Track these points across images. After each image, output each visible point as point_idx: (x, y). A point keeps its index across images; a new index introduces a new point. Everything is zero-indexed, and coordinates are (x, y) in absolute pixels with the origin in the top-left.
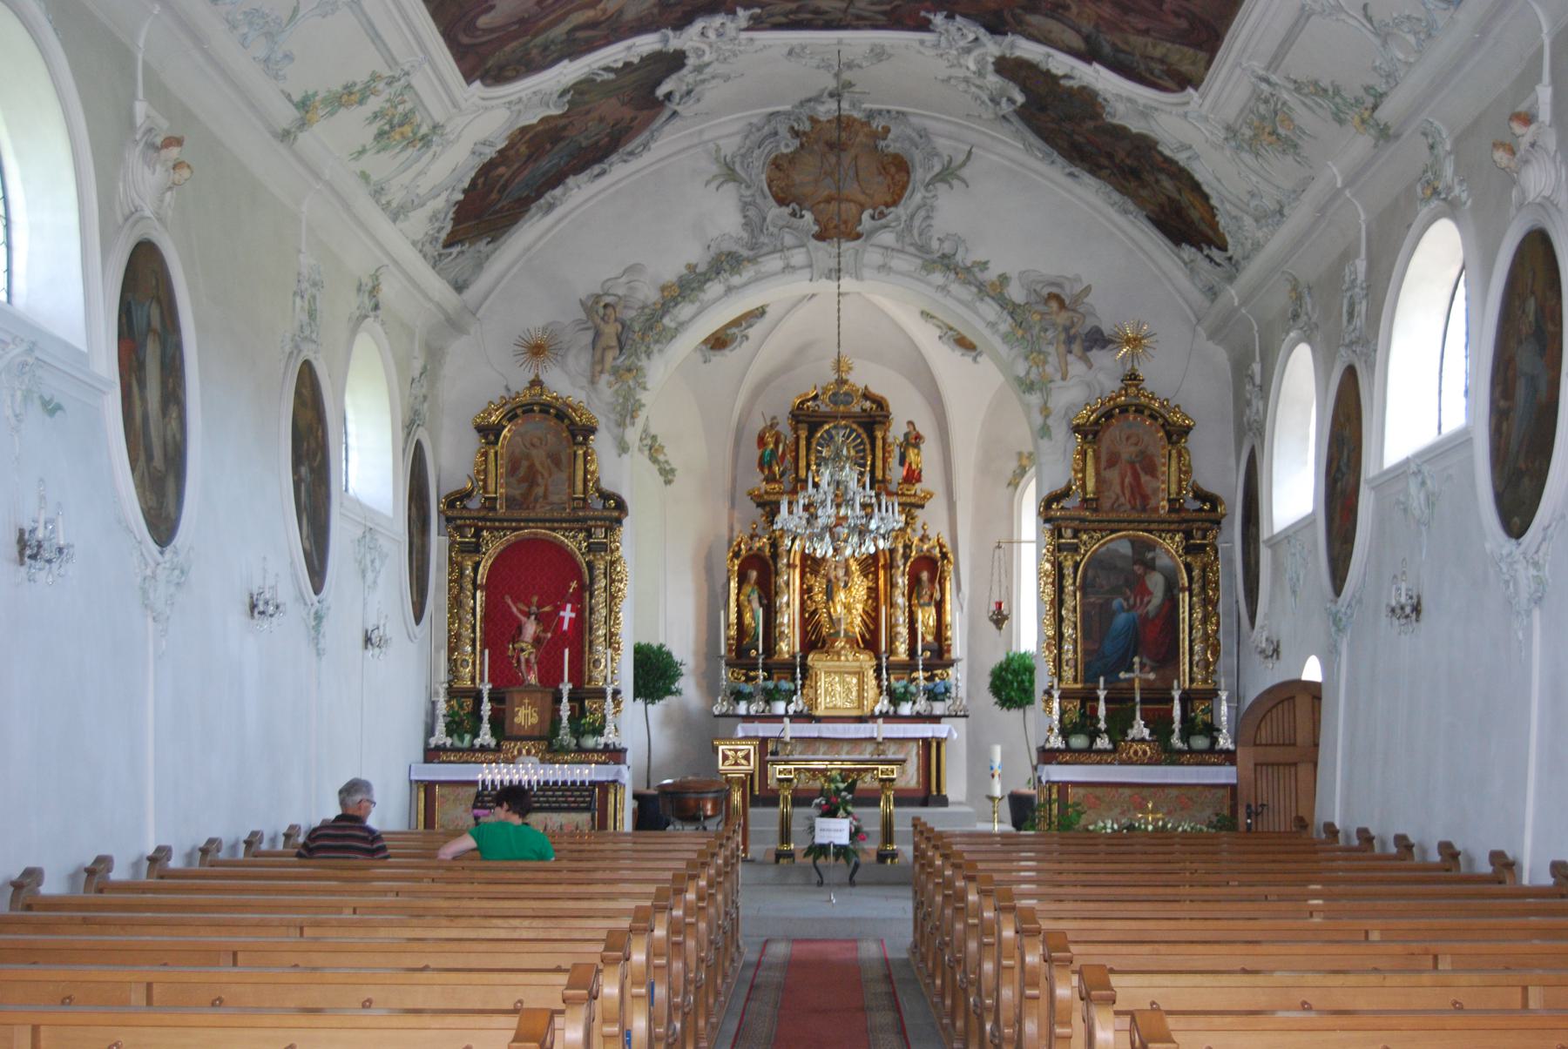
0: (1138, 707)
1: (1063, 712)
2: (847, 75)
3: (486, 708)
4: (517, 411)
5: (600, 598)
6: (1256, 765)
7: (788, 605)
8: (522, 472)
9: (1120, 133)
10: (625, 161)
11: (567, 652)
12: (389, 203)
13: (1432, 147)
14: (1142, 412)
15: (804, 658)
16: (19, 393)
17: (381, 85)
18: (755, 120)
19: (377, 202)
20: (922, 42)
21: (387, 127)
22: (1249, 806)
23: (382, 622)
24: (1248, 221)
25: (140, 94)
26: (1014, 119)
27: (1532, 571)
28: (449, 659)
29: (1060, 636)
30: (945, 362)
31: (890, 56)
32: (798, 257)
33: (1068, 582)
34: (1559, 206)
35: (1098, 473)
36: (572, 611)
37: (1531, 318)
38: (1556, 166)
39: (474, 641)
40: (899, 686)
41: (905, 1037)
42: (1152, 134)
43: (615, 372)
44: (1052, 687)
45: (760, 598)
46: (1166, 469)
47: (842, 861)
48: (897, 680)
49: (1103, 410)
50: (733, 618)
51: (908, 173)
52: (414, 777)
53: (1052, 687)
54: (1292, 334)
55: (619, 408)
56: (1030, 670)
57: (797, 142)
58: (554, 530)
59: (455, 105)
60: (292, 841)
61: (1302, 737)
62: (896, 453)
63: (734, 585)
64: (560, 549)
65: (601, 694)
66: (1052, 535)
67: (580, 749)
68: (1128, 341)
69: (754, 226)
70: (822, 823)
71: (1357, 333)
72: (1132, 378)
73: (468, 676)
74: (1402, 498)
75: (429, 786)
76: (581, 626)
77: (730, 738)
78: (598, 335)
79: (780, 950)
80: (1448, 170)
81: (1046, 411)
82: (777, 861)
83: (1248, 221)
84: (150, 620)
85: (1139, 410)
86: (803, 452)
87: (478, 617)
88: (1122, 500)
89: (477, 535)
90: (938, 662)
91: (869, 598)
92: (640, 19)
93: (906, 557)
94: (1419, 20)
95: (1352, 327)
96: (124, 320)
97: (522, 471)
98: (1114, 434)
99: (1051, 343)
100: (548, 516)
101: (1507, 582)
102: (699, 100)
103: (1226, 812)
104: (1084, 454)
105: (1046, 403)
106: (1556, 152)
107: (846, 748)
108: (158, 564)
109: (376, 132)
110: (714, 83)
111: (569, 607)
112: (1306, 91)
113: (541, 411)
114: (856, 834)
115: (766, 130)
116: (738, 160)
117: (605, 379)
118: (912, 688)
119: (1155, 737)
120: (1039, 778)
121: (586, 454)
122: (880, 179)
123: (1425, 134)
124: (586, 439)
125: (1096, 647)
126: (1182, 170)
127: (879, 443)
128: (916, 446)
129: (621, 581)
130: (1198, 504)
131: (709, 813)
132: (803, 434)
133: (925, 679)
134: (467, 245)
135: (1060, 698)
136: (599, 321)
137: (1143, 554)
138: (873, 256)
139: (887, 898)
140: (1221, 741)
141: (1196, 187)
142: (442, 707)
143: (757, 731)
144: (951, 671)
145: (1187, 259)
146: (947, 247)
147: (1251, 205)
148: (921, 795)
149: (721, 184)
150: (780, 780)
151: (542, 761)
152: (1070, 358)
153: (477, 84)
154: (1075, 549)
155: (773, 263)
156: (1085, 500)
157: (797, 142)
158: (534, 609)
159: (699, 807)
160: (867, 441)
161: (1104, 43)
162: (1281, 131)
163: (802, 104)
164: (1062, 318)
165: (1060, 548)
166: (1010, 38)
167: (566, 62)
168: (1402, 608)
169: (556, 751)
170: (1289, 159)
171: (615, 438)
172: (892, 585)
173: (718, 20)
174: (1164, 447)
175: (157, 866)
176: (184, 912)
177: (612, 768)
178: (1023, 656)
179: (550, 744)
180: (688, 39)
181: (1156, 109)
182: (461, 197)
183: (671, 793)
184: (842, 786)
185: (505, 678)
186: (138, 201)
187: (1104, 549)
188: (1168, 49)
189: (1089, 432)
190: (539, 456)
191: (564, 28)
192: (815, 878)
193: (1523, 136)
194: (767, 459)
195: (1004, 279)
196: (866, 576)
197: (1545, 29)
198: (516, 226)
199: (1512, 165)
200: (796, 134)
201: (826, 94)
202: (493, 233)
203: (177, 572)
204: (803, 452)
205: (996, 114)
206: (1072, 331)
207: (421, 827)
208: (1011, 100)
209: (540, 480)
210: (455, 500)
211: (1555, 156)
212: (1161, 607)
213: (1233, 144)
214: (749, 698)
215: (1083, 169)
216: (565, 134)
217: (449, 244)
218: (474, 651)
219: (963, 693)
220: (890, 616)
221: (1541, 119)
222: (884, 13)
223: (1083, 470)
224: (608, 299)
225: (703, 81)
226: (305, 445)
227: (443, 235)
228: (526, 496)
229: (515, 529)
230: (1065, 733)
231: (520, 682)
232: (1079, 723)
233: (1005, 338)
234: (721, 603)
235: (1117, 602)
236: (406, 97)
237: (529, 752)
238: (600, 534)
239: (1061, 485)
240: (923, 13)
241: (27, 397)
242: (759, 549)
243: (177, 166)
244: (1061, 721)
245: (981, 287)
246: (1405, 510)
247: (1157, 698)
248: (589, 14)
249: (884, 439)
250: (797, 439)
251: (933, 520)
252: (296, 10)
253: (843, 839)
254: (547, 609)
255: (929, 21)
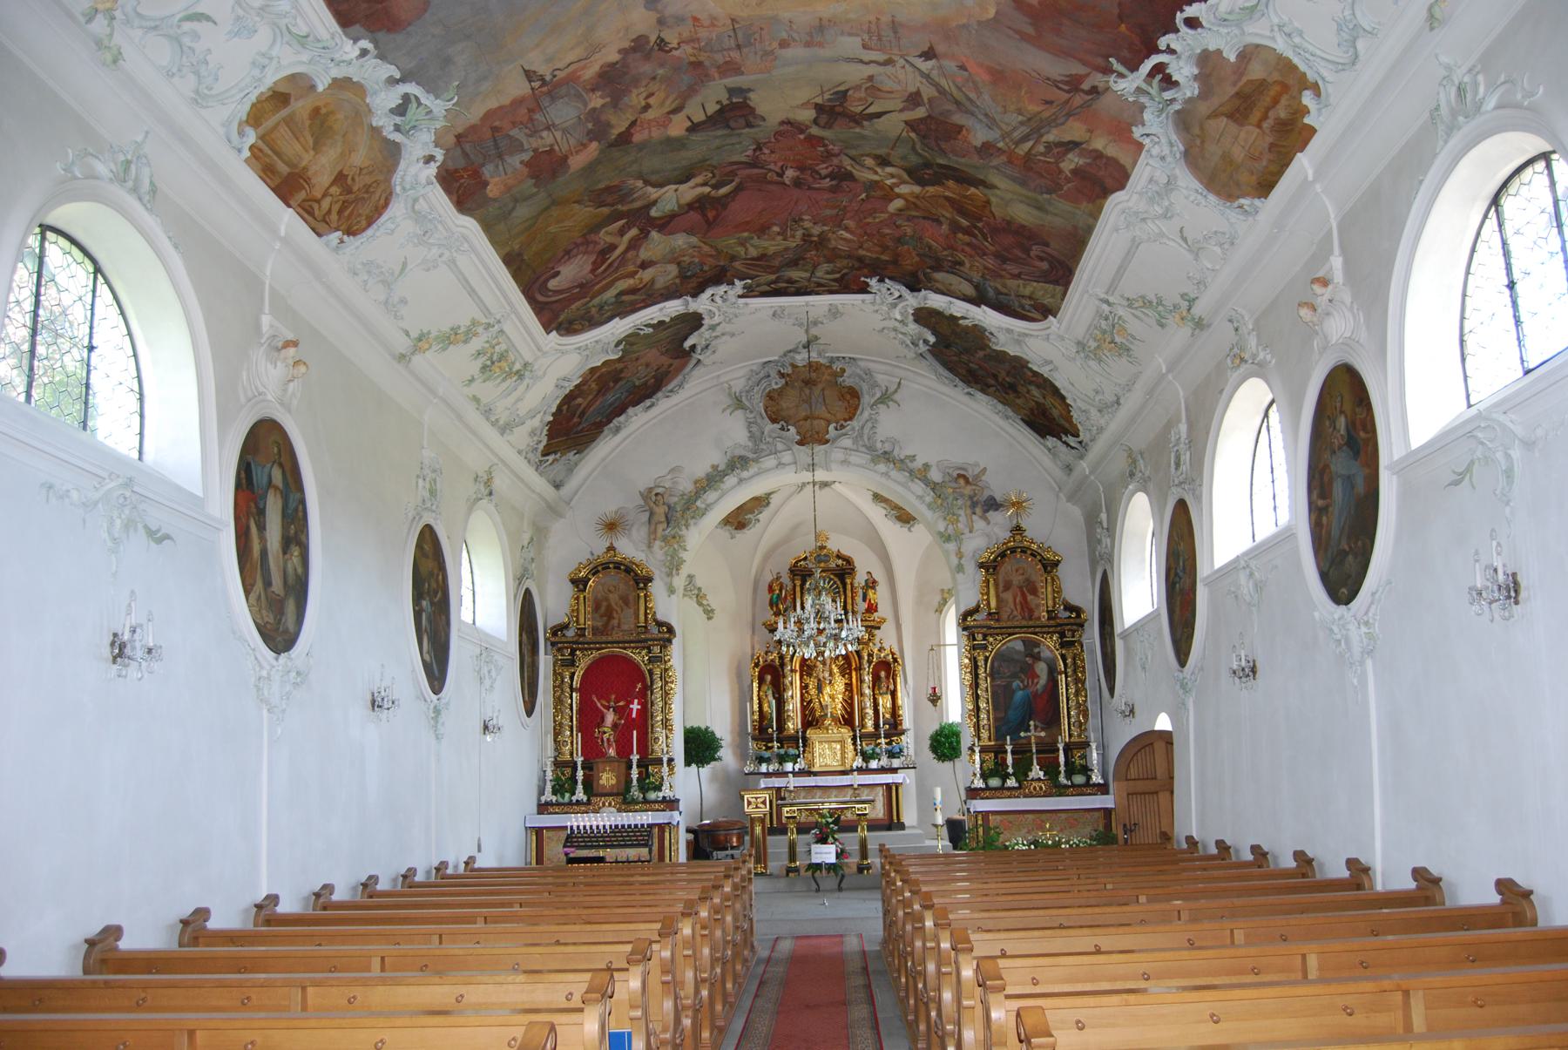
0: (1035, 756)
1: (982, 762)
2: (814, 331)
3: (580, 774)
4: (599, 568)
5: (658, 694)
6: (1128, 794)
7: (792, 697)
8: (603, 609)
9: (1001, 357)
10: (667, 397)
11: (635, 732)
12: (497, 420)
13: (1237, 330)
14: (1025, 552)
15: (804, 732)
16: (118, 522)
17: (480, 329)
18: (754, 368)
19: (488, 419)
20: (863, 301)
21: (489, 363)
22: (1125, 826)
23: (495, 715)
24: (1094, 412)
25: (267, 309)
26: (929, 356)
27: (1364, 629)
28: (555, 741)
29: (978, 708)
30: (889, 530)
31: (842, 314)
32: (787, 457)
33: (981, 671)
34: (1361, 341)
35: (998, 596)
36: (638, 704)
37: (1343, 432)
38: (1353, 313)
39: (571, 727)
40: (868, 749)
41: (879, 1034)
42: (1024, 356)
43: (664, 539)
44: (974, 745)
45: (773, 693)
46: (1044, 590)
47: (832, 873)
48: (867, 745)
49: (998, 552)
50: (756, 707)
51: (859, 398)
52: (528, 825)
53: (974, 745)
54: (1130, 487)
55: (668, 564)
56: (957, 735)
57: (783, 381)
58: (625, 648)
59: (539, 349)
60: (469, 867)
61: (1161, 772)
62: (860, 593)
63: (755, 685)
64: (629, 662)
65: (659, 762)
66: (969, 639)
67: (645, 801)
68: (1013, 504)
69: (756, 438)
70: (816, 848)
71: (1184, 476)
72: (1018, 529)
73: (567, 752)
74: (1233, 589)
75: (539, 831)
76: (645, 713)
77: (756, 789)
78: (652, 514)
79: (786, 946)
80: (1252, 342)
81: (960, 555)
82: (787, 875)
83: (1094, 412)
84: (265, 711)
85: (1024, 551)
86: (798, 594)
87: (574, 712)
88: (1015, 613)
89: (573, 653)
90: (893, 731)
91: (846, 690)
92: (667, 288)
93: (870, 662)
94: (1224, 233)
95: (1179, 473)
96: (243, 475)
97: (604, 610)
98: (1007, 567)
99: (960, 508)
100: (621, 639)
101: (1339, 641)
102: (714, 352)
103: (1101, 828)
104: (987, 582)
105: (959, 548)
106: (1352, 303)
107: (834, 792)
108: (273, 667)
109: (481, 366)
110: (724, 338)
111: (636, 701)
112: (1136, 305)
113: (615, 568)
114: (840, 854)
115: (762, 375)
116: (744, 394)
117: (658, 543)
118: (878, 750)
119: (1047, 777)
120: (968, 809)
121: (646, 596)
122: (840, 403)
123: (1230, 321)
124: (646, 585)
125: (1002, 715)
126: (1046, 380)
127: (849, 587)
128: (873, 588)
129: (672, 682)
130: (1067, 614)
131: (735, 844)
132: (798, 583)
133: (886, 743)
134: (559, 454)
135: (980, 752)
136: (652, 504)
137: (1030, 645)
138: (838, 455)
139: (864, 900)
140: (1094, 778)
141: (1056, 391)
142: (549, 776)
143: (773, 782)
144: (903, 737)
145: (1050, 446)
146: (887, 447)
147: (1097, 399)
148: (887, 823)
149: (733, 411)
150: (788, 818)
151: (619, 811)
152: (974, 517)
153: (554, 333)
154: (985, 648)
155: (770, 462)
156: (990, 614)
157: (783, 381)
158: (612, 704)
159: (728, 840)
160: (841, 586)
161: (989, 289)
162: (1118, 339)
163: (785, 355)
164: (968, 490)
165: (974, 648)
166: (923, 292)
167: (617, 319)
168: (1243, 670)
169: (629, 803)
170: (1124, 360)
171: (666, 584)
172: (862, 681)
173: (723, 288)
174: (1042, 576)
175: (408, 881)
176: (291, 944)
177: (668, 813)
178: (951, 725)
179: (625, 799)
180: (701, 304)
181: (1026, 335)
182: (551, 418)
183: (707, 831)
184: (830, 820)
185: (593, 751)
186: (261, 389)
187: (1004, 647)
188: (1035, 288)
189: (990, 567)
190: (614, 598)
191: (610, 294)
192: (814, 886)
193: (1323, 295)
194: (775, 600)
195: (927, 466)
196: (843, 676)
197: (1332, 216)
198: (594, 444)
199: (1315, 319)
200: (782, 375)
201: (800, 346)
202: (578, 447)
203: (293, 674)
204: (798, 594)
205: (916, 353)
206: (975, 499)
207: (534, 861)
208: (926, 342)
209: (615, 615)
210: (558, 630)
211: (1352, 307)
212: (1045, 686)
213: (1082, 355)
214: (768, 761)
215: (977, 389)
216: (622, 375)
217: (545, 454)
218: (572, 735)
219: (911, 752)
220: (860, 702)
221: (1335, 281)
222: (835, 280)
223: (988, 594)
224: (660, 490)
225: (716, 337)
226: (427, 585)
227: (541, 447)
228: (606, 625)
229: (598, 649)
230: (985, 776)
231: (604, 755)
232: (995, 769)
233: (929, 506)
234: (748, 698)
235: (1016, 684)
236: (500, 340)
237: (610, 805)
238: (656, 650)
239: (973, 604)
240: (862, 279)
241: (129, 525)
242: (772, 660)
243: (296, 363)
244: (981, 768)
245: (911, 472)
246: (1236, 597)
247: (1048, 749)
248: (630, 282)
249: (852, 584)
250: (795, 586)
251: (886, 638)
252: (405, 265)
253: (832, 859)
254: (621, 704)
255: (867, 285)
